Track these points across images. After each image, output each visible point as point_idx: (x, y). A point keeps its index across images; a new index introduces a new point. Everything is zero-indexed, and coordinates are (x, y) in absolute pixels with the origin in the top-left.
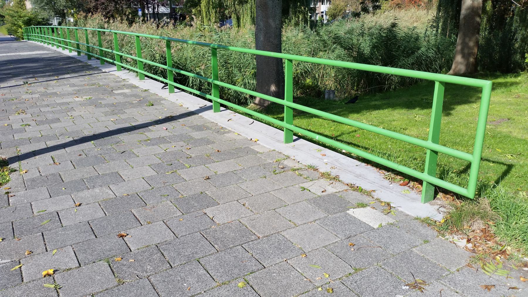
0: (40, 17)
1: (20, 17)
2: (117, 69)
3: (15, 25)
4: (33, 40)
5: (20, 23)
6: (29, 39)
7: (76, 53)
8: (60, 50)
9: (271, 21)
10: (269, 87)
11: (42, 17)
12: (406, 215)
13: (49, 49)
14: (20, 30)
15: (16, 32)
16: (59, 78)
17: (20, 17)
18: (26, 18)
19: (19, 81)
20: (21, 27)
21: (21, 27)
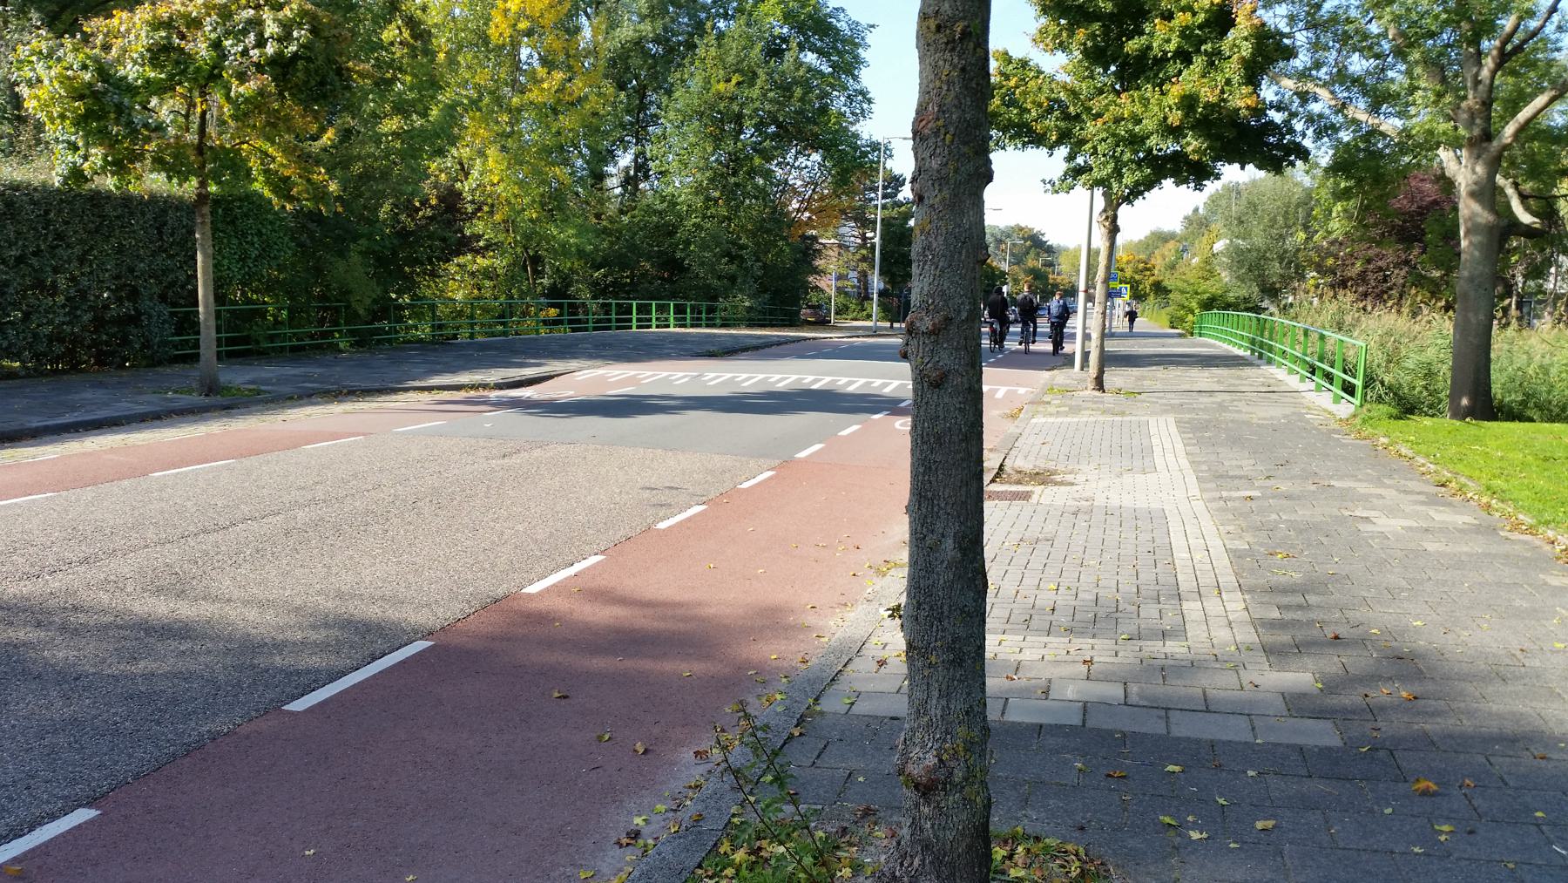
0: (1231, 295)
1: (1197, 293)
2: (1313, 388)
3: (1184, 307)
4: (1210, 336)
5: (1194, 305)
6: (1200, 335)
7: (1249, 352)
8: (1230, 348)
9: (1471, 315)
10: (1460, 399)
11: (1237, 295)
12: (920, 171)
13: (1219, 347)
14: (1190, 317)
15: (1182, 320)
16: (1095, 224)
17: (1197, 293)
18: (1206, 296)
19: (1161, 368)
20: (1192, 312)
21: (1192, 312)
